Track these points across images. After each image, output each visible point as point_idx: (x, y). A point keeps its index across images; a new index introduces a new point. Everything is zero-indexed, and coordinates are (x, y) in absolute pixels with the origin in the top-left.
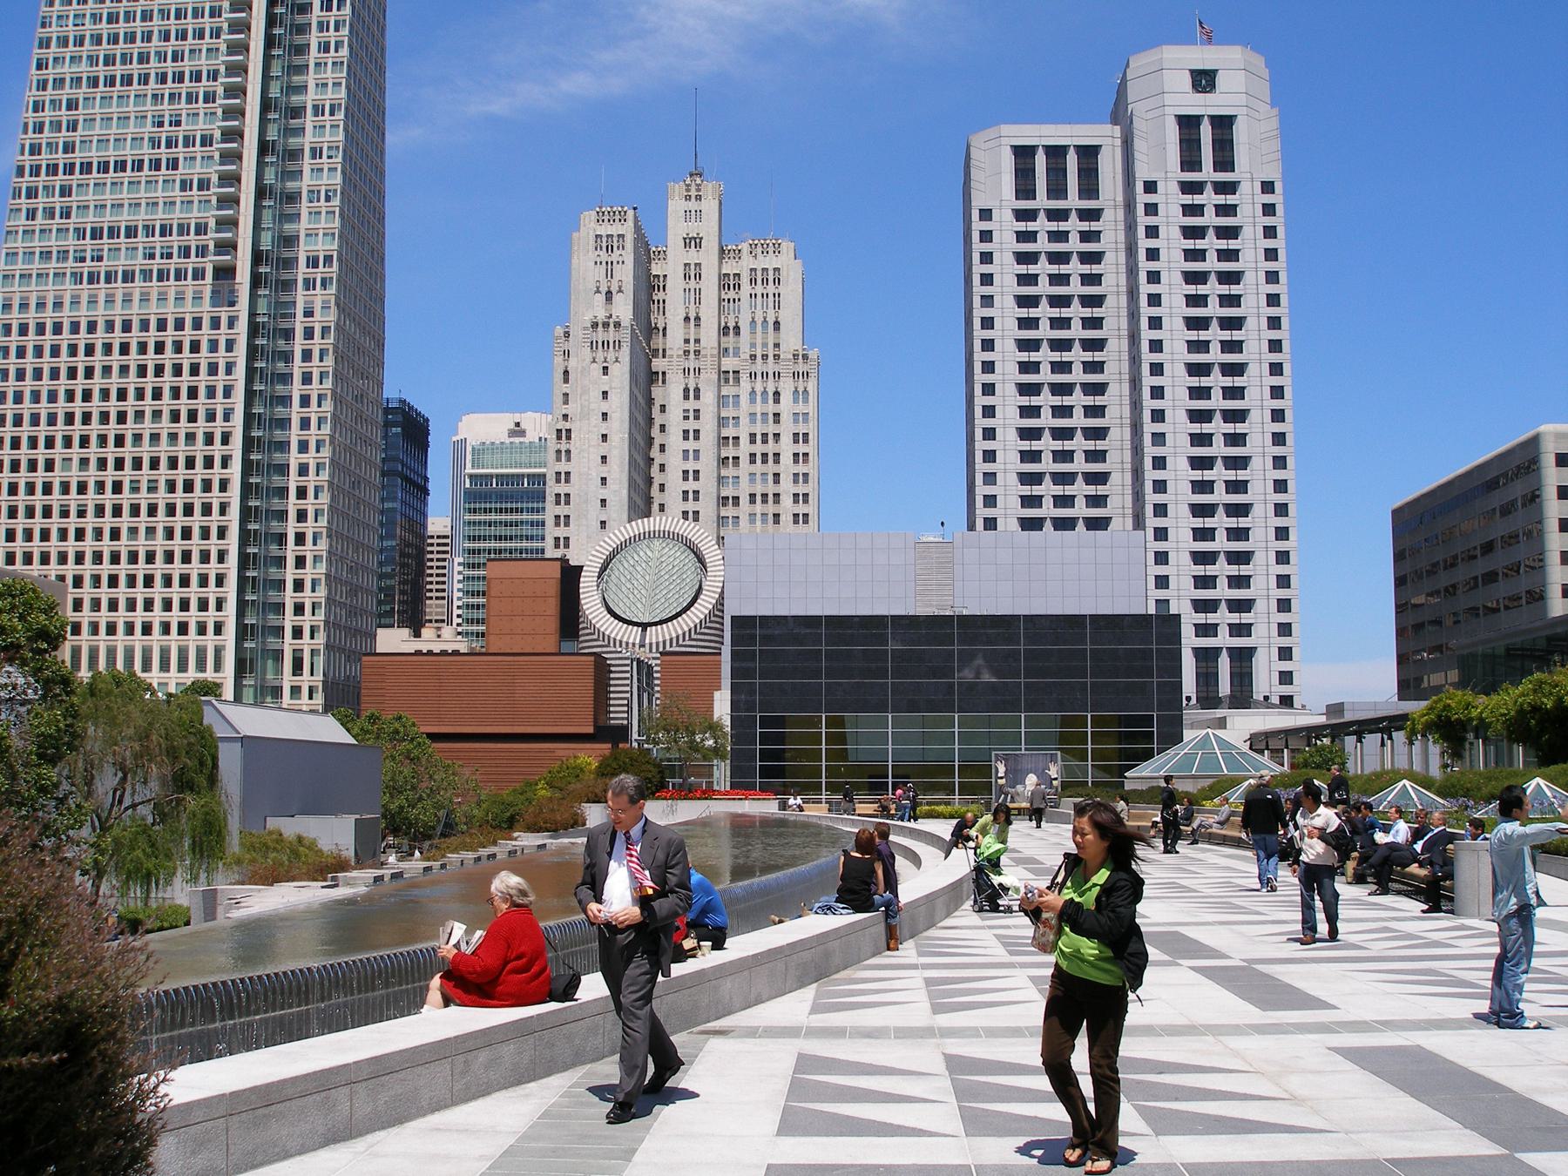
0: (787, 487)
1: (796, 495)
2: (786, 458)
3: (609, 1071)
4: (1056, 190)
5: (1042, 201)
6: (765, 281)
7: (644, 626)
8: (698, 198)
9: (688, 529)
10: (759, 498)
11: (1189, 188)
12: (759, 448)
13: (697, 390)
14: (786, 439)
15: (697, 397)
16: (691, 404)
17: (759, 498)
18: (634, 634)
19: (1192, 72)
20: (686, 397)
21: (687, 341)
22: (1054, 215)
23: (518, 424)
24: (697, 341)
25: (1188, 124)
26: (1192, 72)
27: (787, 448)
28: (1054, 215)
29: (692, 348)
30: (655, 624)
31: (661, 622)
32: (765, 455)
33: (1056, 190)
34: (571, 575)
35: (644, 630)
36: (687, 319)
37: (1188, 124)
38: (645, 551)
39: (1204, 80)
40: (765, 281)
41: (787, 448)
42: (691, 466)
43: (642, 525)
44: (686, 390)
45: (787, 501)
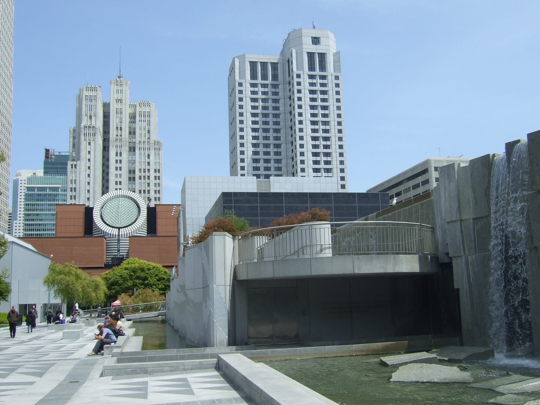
0: (152, 188)
1: (155, 191)
2: (152, 178)
3: (495, 158)
4: (265, 77)
5: (259, 81)
6: (144, 116)
7: (119, 228)
8: (121, 85)
9: (131, 194)
10: (142, 192)
11: (311, 77)
12: (143, 174)
13: (121, 153)
14: (152, 171)
15: (121, 155)
16: (119, 158)
17: (142, 192)
18: (115, 232)
19: (312, 37)
20: (117, 155)
21: (117, 136)
22: (264, 86)
23: (34, 174)
24: (121, 136)
25: (311, 55)
26: (312, 37)
27: (152, 174)
28: (264, 86)
29: (119, 138)
30: (123, 228)
31: (125, 227)
32: (144, 177)
33: (265, 77)
34: (89, 211)
35: (119, 230)
36: (117, 128)
37: (311, 55)
38: (108, 205)
39: (316, 41)
40: (144, 116)
41: (152, 174)
42: (118, 180)
43: (107, 196)
44: (117, 153)
45: (152, 193)
